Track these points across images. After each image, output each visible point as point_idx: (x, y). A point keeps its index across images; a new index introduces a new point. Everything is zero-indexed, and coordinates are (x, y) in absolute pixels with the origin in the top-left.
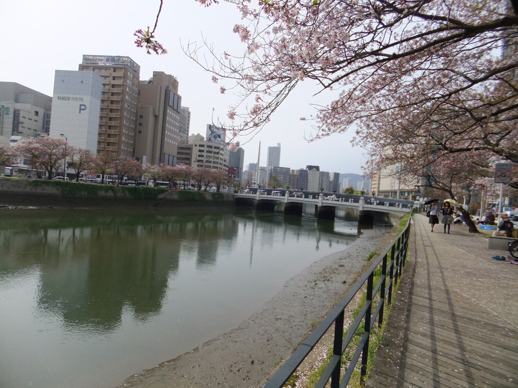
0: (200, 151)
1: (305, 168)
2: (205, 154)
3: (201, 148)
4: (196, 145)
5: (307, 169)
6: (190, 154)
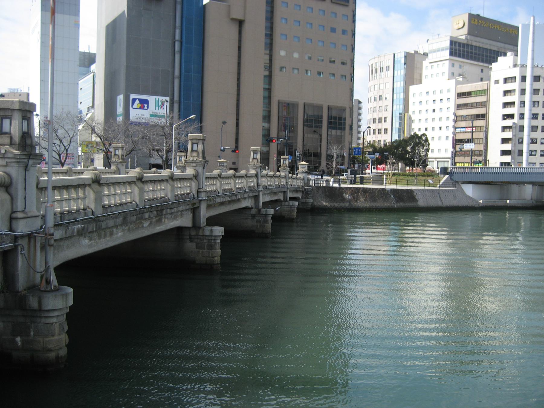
0: (506, 93)
3: (509, 86)
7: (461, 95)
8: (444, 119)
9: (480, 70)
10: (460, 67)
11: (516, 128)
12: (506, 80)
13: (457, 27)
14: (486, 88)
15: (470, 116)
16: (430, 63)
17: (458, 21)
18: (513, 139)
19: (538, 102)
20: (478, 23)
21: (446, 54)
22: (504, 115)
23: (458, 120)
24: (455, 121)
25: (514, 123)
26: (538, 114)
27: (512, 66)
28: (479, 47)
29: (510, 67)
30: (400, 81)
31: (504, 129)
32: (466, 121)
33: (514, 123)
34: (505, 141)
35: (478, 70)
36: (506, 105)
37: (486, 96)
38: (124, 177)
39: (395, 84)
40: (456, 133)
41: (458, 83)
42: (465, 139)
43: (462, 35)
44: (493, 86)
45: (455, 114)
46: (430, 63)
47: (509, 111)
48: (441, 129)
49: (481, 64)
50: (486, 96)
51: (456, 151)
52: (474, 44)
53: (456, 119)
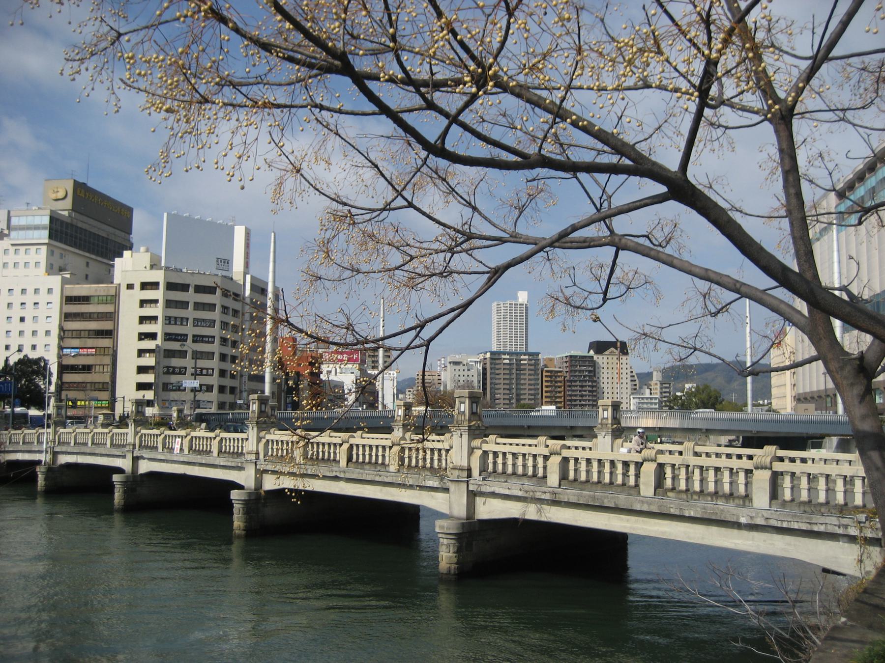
0: (143, 303)
1: (582, 350)
2: (190, 313)
3: (149, 294)
4: (130, 287)
5: (592, 353)
6: (112, 316)
7: (70, 300)
8: (41, 333)
9: (85, 264)
10: (62, 256)
11: (159, 352)
12: (145, 286)
13: (54, 196)
14: (114, 294)
15: (87, 332)
16: (13, 245)
17: (57, 188)
18: (157, 368)
19: (187, 319)
20: (85, 195)
21: (43, 236)
22: (140, 334)
23: (66, 336)
24: (61, 338)
25: (157, 346)
26: (187, 335)
27: (148, 267)
28: (85, 230)
31: (141, 353)
32: (80, 338)
33: (157, 346)
34: (141, 370)
36: (143, 320)
40: (63, 355)
41: (64, 282)
42: (78, 366)
44: (124, 293)
45: (61, 329)
46: (13, 245)
47: (148, 328)
48: (34, 349)
49: (87, 254)
51: (63, 383)
52: (80, 225)
53: (62, 334)
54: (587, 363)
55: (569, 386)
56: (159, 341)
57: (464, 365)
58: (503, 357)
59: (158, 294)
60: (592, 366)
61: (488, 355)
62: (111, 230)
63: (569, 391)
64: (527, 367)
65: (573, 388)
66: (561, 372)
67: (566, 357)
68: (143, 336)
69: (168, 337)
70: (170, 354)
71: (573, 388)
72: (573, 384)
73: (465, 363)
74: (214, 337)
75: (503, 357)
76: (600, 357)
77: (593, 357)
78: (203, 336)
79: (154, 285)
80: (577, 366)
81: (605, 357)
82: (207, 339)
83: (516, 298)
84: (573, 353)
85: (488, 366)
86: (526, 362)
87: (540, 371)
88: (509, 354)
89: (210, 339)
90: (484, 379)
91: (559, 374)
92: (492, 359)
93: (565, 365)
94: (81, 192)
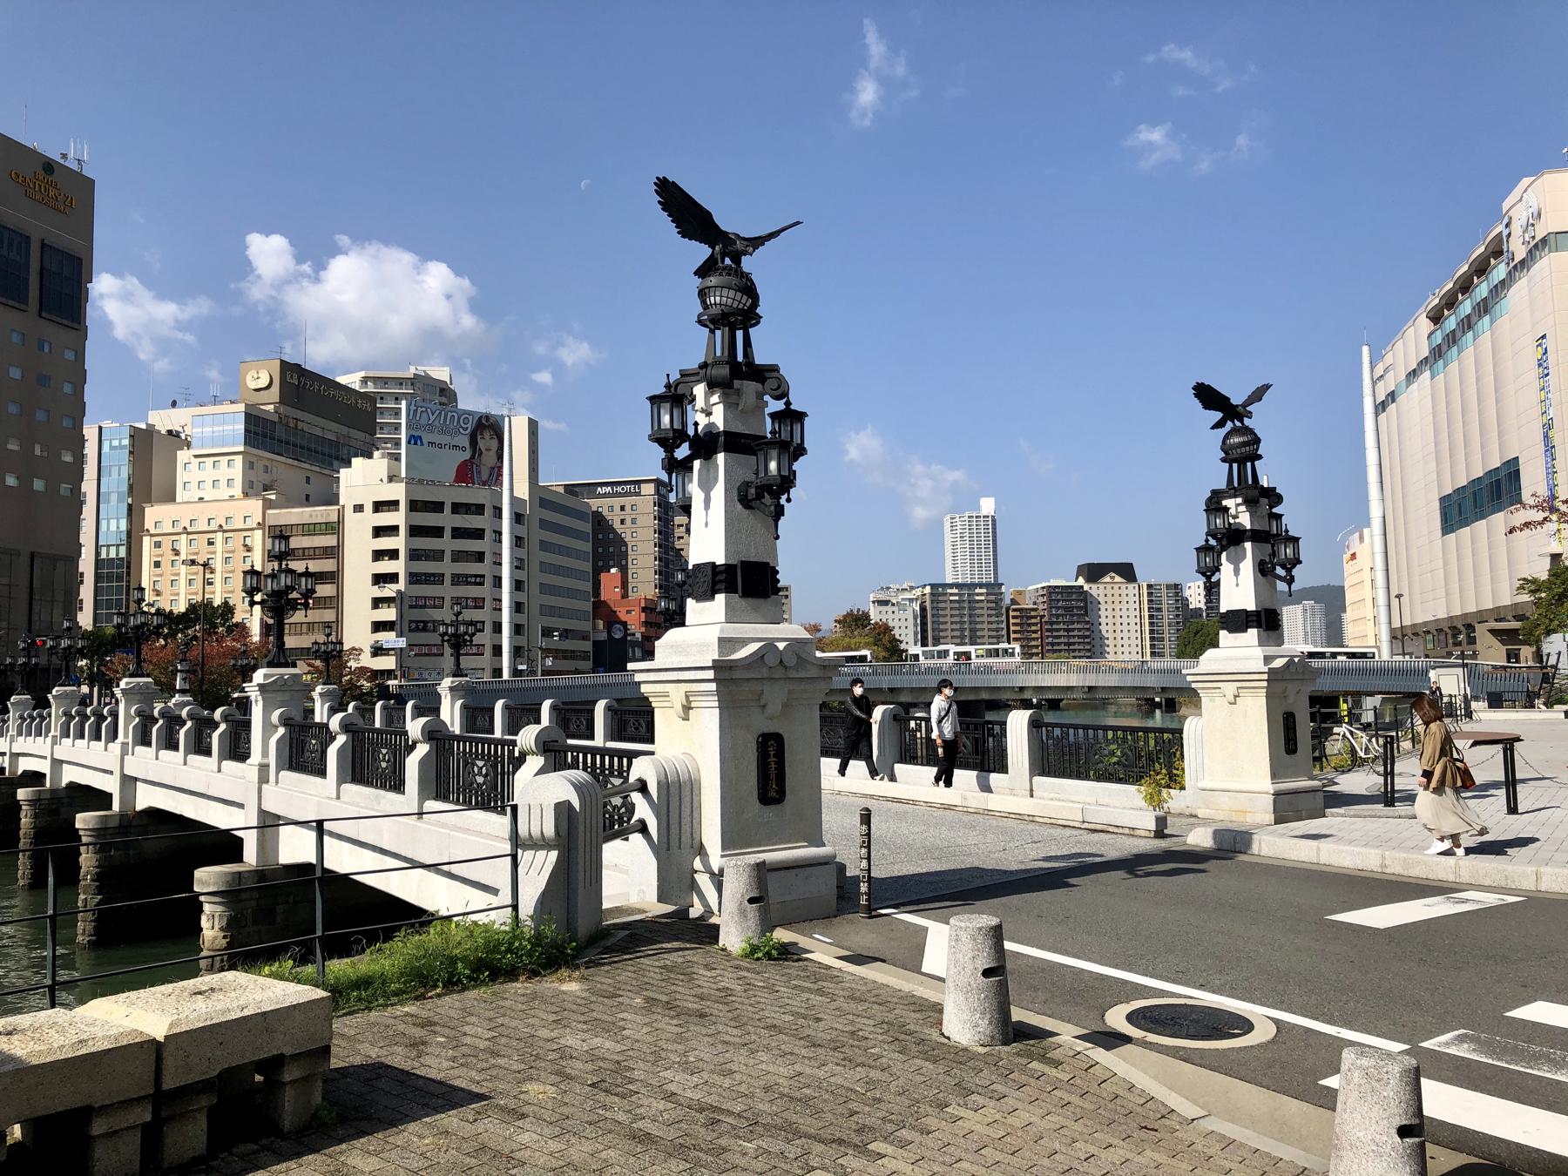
0: (379, 532)
1: (341, 503)
3: (386, 519)
4: (359, 508)
5: (1081, 581)
6: (335, 552)
12: (379, 506)
16: (196, 456)
25: (399, 592)
27: (385, 480)
29: (381, 480)
30: (118, 519)
31: (377, 603)
35: (302, 476)
36: (378, 555)
37: (336, 536)
38: (1049, 950)
39: (103, 524)
41: (268, 505)
43: (269, 404)
44: (351, 518)
46: (196, 456)
50: (336, 536)
54: (1074, 597)
55: (1048, 630)
56: (401, 585)
57: (893, 605)
58: (949, 591)
59: (398, 518)
60: (1082, 600)
61: (928, 590)
62: (344, 430)
63: (1048, 637)
64: (985, 605)
65: (1055, 634)
66: (1035, 610)
67: (1043, 588)
68: (379, 579)
69: (414, 578)
70: (419, 603)
71: (1055, 634)
72: (1055, 627)
73: (895, 601)
74: (483, 576)
75: (949, 591)
76: (1094, 586)
77: (1082, 587)
78: (467, 576)
79: (392, 505)
80: (1059, 600)
81: (1101, 586)
82: (473, 580)
83: (979, 509)
84: (1053, 583)
85: (928, 604)
86: (983, 598)
87: (1004, 611)
88: (957, 585)
89: (478, 580)
90: (924, 624)
91: (1033, 613)
92: (932, 594)
93: (1041, 599)
94: (292, 377)
